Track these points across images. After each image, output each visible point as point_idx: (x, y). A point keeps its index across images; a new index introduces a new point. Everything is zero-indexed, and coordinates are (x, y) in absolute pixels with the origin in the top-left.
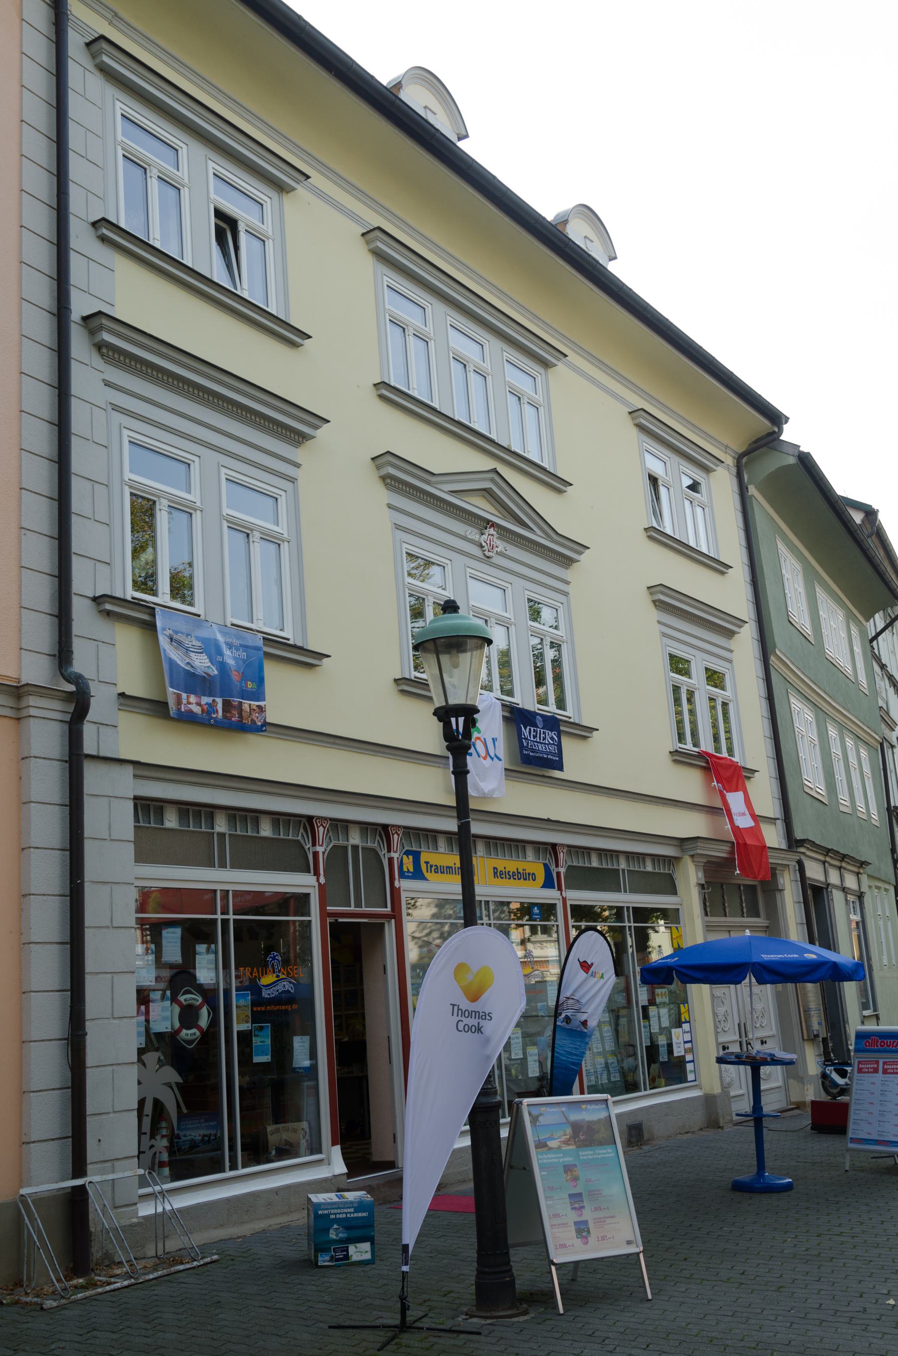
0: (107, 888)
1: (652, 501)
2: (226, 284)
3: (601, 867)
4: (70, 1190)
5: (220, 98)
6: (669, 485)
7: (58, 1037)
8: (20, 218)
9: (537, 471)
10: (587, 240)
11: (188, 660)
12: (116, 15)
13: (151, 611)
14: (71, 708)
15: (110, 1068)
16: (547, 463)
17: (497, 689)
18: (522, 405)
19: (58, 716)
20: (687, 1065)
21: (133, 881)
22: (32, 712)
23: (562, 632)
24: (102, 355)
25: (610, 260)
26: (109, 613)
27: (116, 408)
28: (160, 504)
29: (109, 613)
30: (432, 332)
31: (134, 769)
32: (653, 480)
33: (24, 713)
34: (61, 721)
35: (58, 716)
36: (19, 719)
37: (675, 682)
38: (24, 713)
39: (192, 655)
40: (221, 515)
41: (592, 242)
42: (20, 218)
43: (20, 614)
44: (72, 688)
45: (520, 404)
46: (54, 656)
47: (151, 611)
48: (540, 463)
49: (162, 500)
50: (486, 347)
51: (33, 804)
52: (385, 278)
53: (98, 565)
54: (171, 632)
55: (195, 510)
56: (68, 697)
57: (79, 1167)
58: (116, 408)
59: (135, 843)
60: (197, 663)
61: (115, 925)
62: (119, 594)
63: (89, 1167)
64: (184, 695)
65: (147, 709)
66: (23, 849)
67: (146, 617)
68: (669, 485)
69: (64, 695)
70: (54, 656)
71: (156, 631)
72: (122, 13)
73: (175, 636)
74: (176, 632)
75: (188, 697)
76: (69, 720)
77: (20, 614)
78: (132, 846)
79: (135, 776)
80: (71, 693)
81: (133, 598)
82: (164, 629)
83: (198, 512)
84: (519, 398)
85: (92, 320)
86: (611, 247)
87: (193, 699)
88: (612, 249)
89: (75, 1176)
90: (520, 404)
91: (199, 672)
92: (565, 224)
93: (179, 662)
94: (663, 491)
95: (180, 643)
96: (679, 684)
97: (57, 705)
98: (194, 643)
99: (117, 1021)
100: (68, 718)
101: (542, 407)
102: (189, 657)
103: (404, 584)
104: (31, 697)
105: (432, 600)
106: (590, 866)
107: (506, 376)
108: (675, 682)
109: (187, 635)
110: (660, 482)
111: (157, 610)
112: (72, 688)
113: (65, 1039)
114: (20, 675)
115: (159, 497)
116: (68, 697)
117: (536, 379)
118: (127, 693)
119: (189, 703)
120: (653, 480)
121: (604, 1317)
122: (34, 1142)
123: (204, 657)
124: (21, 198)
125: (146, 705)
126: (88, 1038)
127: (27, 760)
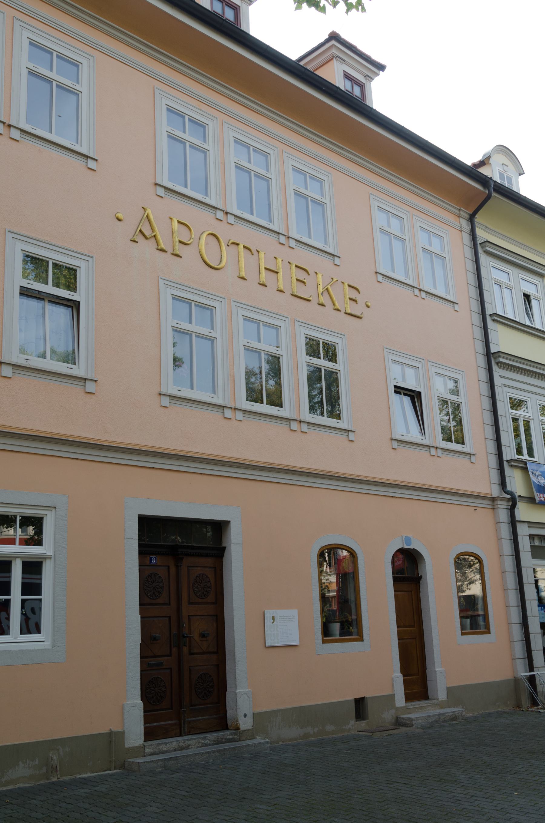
0: (525, 568)
1: (526, 309)
2: (528, 323)
3: (541, 545)
4: (529, 677)
5: (529, 250)
6: (539, 299)
7: (519, 622)
8: (472, 321)
9: (536, 332)
10: (504, 165)
11: (538, 481)
12: (486, 227)
13: (525, 463)
14: (510, 503)
15: (533, 634)
16: (518, 319)
17: (526, 455)
18: (502, 289)
19: (505, 507)
20: (544, 666)
21: (532, 566)
22: (499, 506)
23: (530, 414)
24: (498, 366)
25: (520, 175)
26: (512, 466)
27: (505, 385)
28: (520, 420)
29: (512, 466)
30: (513, 284)
31: (528, 524)
32: (527, 297)
33: (496, 507)
34: (507, 509)
35: (505, 507)
36: (493, 509)
37: (513, 415)
38: (496, 507)
39: (539, 478)
40: (539, 420)
41: (507, 166)
42: (472, 321)
43: (489, 470)
44: (509, 496)
45: (501, 289)
46: (499, 484)
47: (525, 463)
48: (514, 319)
49: (521, 418)
50: (511, 274)
51: (503, 540)
52: (491, 263)
53: (507, 447)
54: (532, 470)
55: (531, 420)
56: (508, 500)
57: (531, 669)
58: (505, 385)
59: (531, 552)
60: (541, 481)
61: (529, 582)
62: (513, 458)
63: (535, 669)
64: (539, 494)
65: (527, 501)
66: (501, 556)
67: (523, 466)
68: (539, 299)
69: (507, 499)
70: (499, 484)
71: (528, 470)
72: (489, 226)
73: (533, 472)
74: (534, 470)
75: (540, 495)
76: (509, 508)
77: (489, 470)
78: (530, 553)
79: (529, 527)
80: (509, 499)
81: (517, 458)
82: (530, 470)
83: (532, 420)
84: (500, 286)
85: (496, 354)
86: (520, 166)
87: (541, 495)
88: (521, 168)
89: (530, 671)
90: (501, 289)
91: (542, 485)
92: (489, 158)
93: (536, 482)
94: (534, 303)
95: (535, 474)
96: (518, 417)
97: (505, 503)
98: (539, 474)
99: (533, 618)
100: (509, 507)
101: (514, 289)
102: (538, 479)
103: (509, 413)
104: (498, 501)
105: (522, 419)
106: (533, 545)
107: (492, 274)
108: (513, 415)
109: (537, 471)
110: (532, 298)
111: (527, 463)
112: (509, 496)
113: (521, 623)
114: (491, 492)
115: (520, 417)
116: (508, 500)
117: (538, 286)
118: (522, 496)
119: (541, 497)
120: (527, 297)
121: (534, 805)
122: (517, 659)
123: (543, 478)
124: (471, 314)
125: (526, 499)
126: (529, 623)
127: (498, 524)
